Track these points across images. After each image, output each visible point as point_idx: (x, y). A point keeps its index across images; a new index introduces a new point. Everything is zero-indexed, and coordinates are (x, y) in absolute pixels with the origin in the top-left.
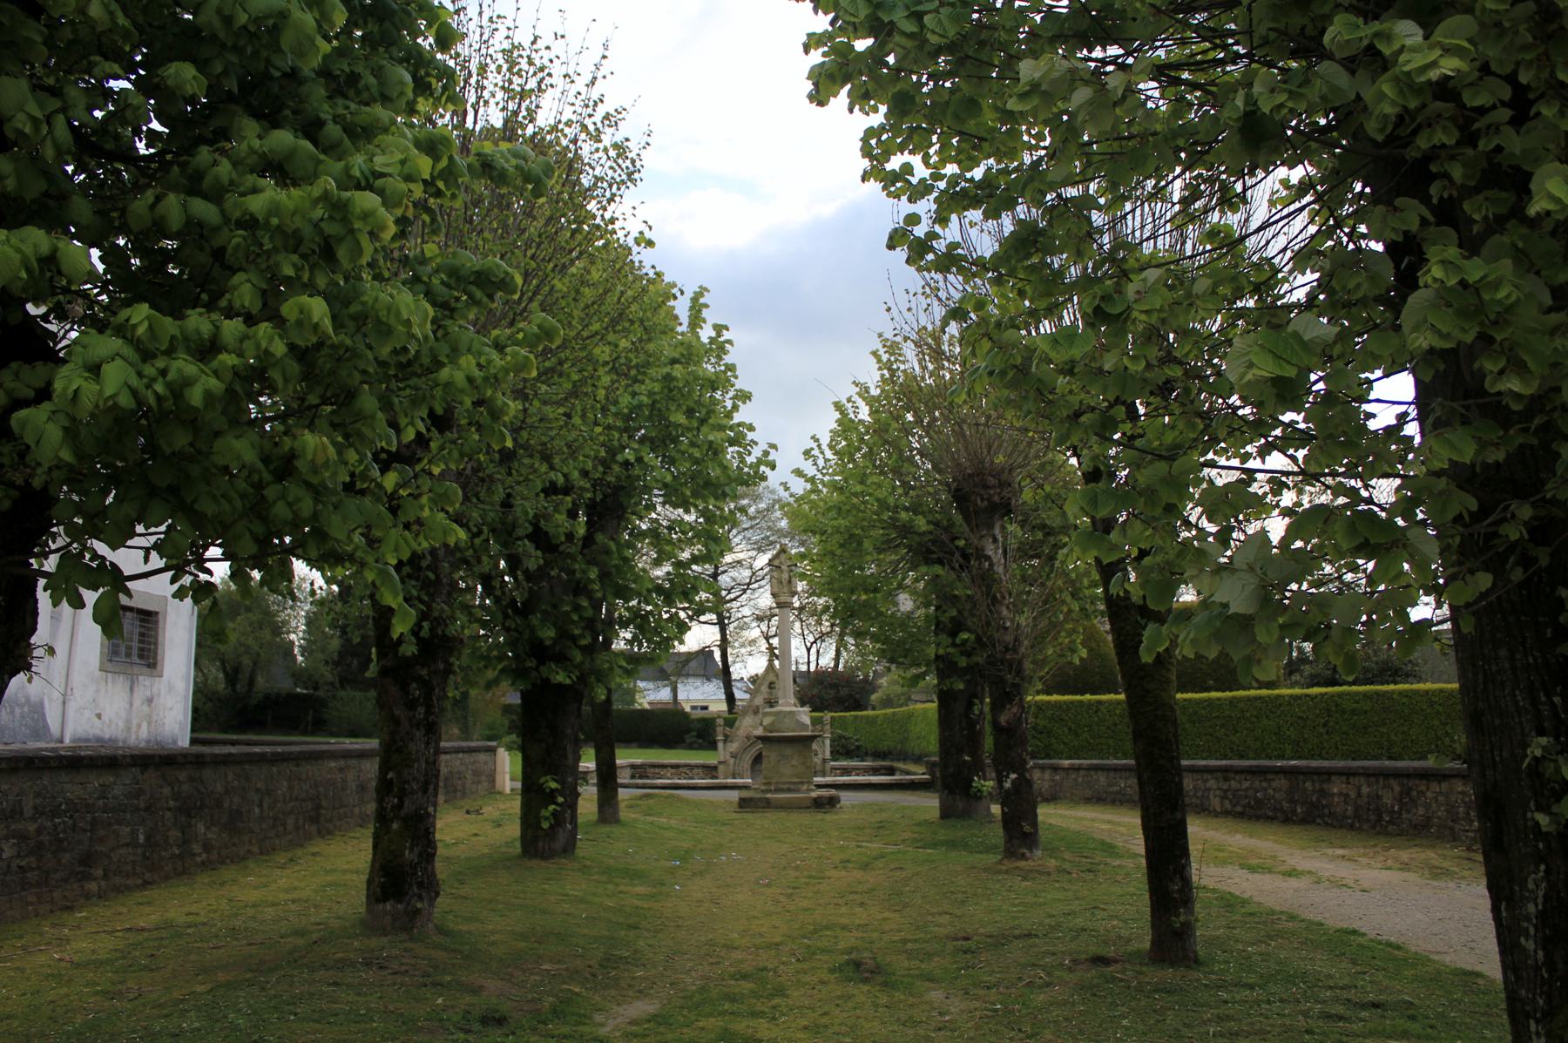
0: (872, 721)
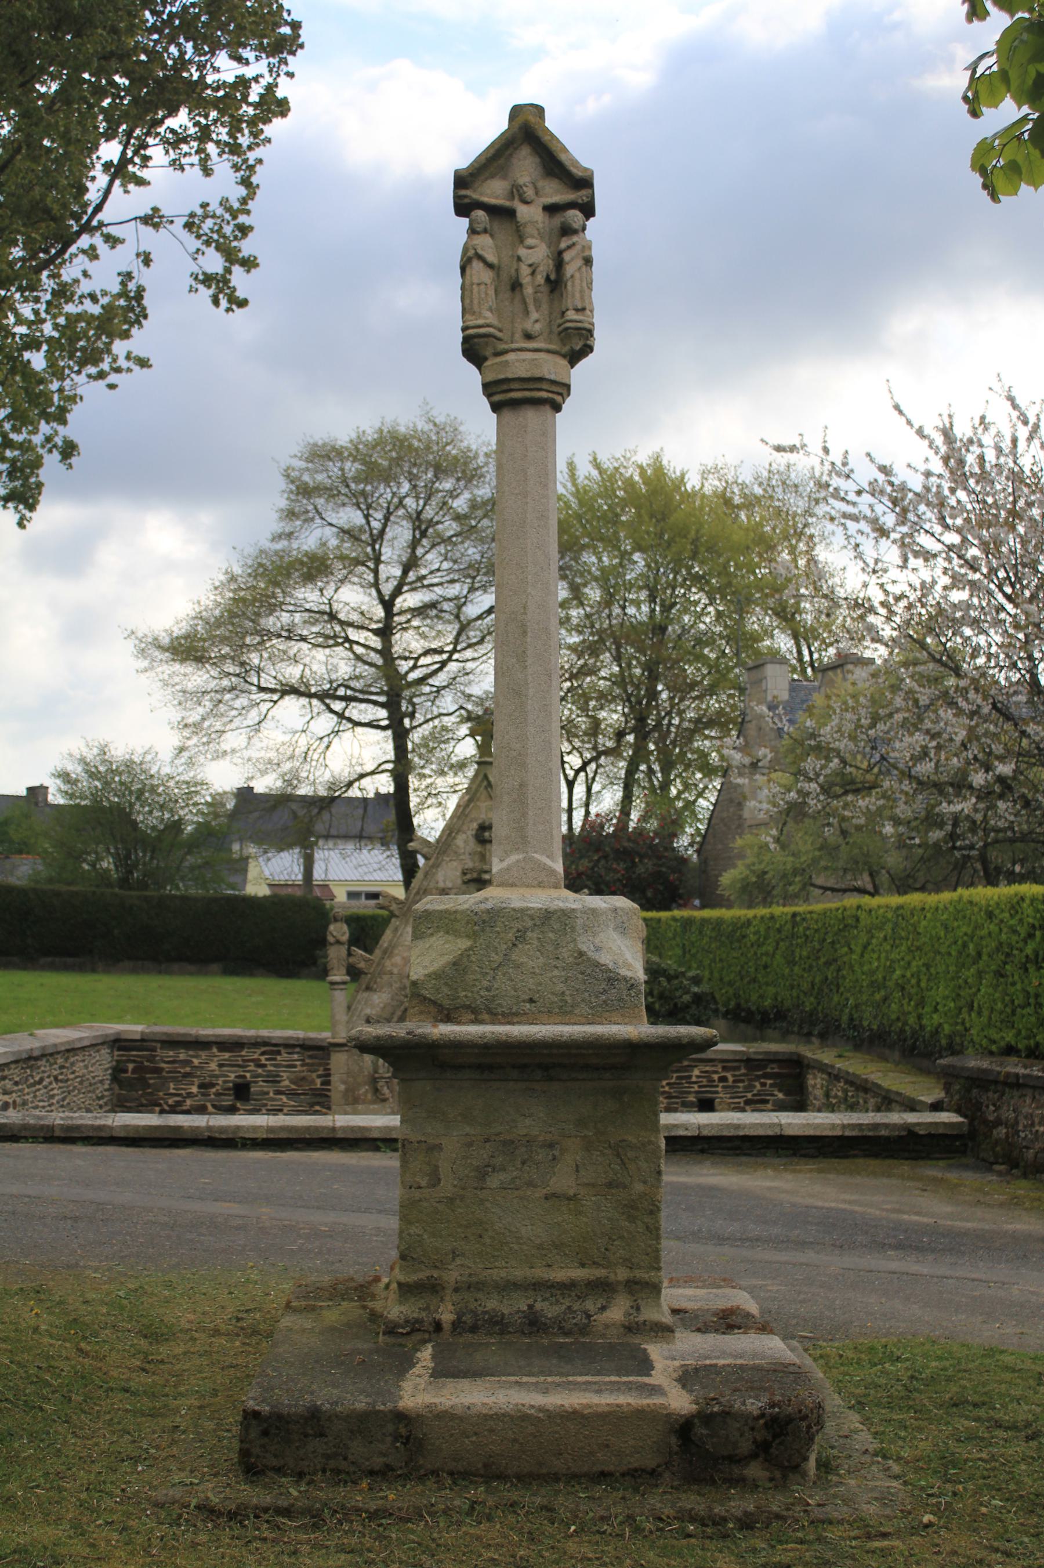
0: (732, 934)
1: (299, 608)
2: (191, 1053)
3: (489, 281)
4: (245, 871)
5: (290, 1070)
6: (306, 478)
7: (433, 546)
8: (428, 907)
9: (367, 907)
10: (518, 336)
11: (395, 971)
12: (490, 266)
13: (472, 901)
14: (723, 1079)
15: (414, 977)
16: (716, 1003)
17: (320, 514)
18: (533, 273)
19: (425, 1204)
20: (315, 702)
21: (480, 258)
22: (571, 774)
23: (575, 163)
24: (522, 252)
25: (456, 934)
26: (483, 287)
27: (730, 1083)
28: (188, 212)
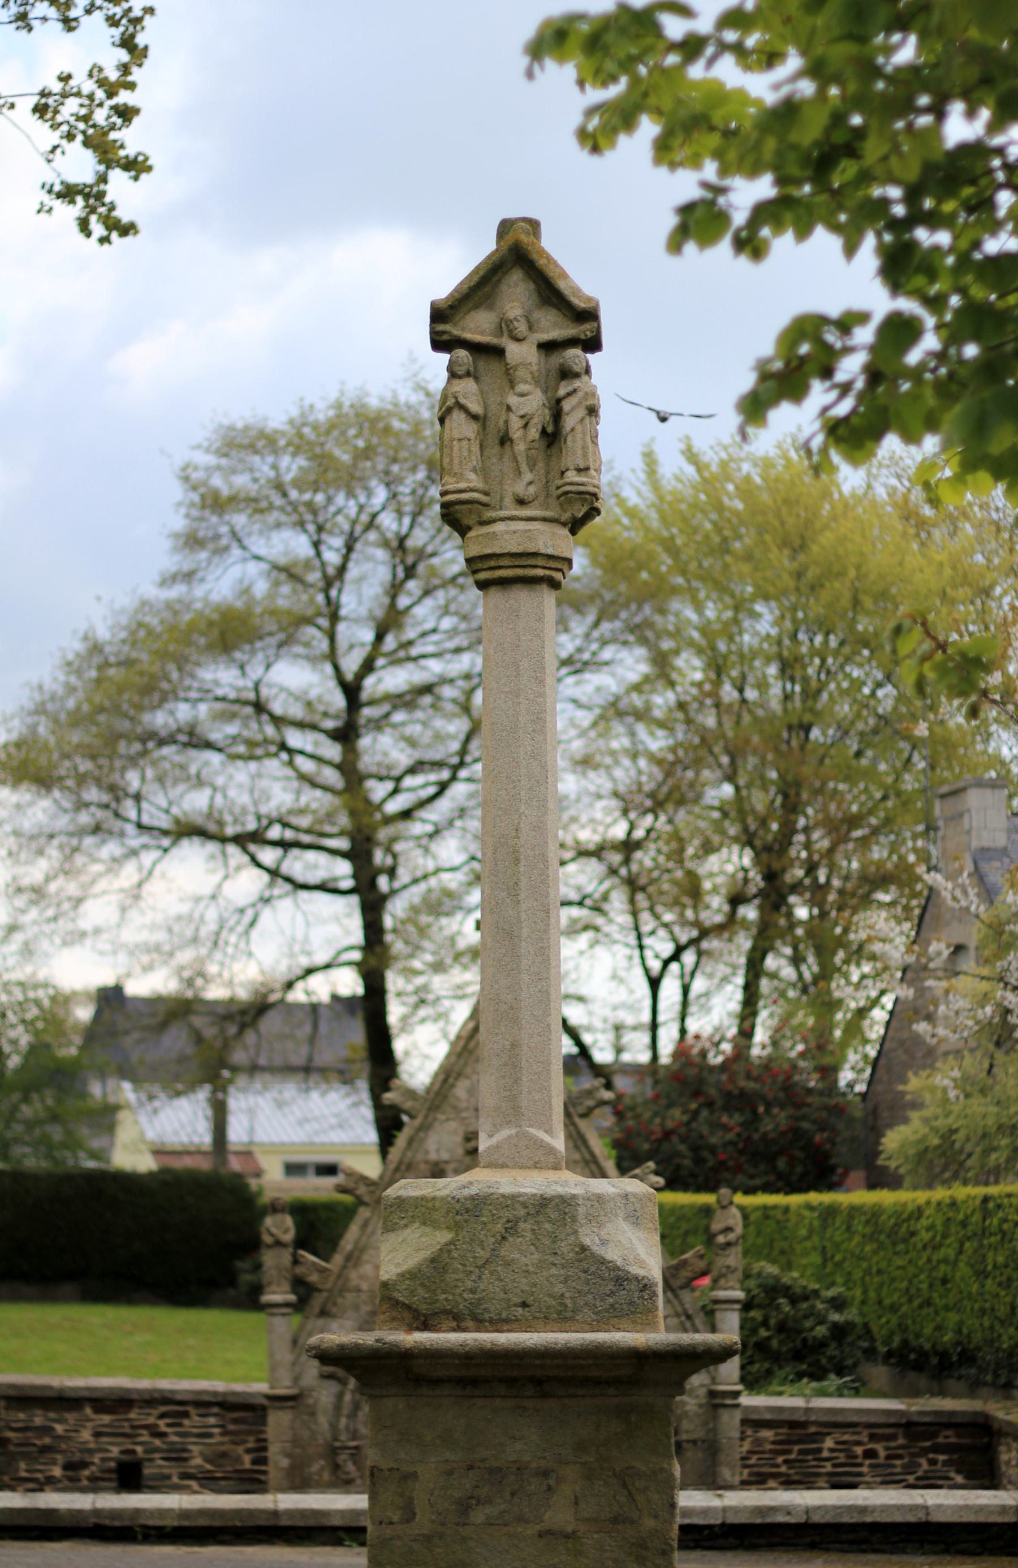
0: (895, 1231)
1: (205, 694)
2: (52, 1415)
3: (472, 436)
4: (110, 1128)
5: (203, 1440)
6: (217, 481)
7: (427, 592)
8: (403, 1193)
9: (318, 1189)
10: (508, 501)
11: (365, 1286)
12: (475, 417)
13: (454, 1185)
14: (870, 1454)
15: (384, 1276)
16: (873, 1340)
17: (239, 541)
18: (525, 426)
19: (398, 1543)
20: (232, 849)
21: (462, 407)
22: (655, 965)
23: (577, 291)
24: (512, 400)
25: (435, 1225)
26: (465, 443)
27: (881, 1460)
28: (38, 89)
